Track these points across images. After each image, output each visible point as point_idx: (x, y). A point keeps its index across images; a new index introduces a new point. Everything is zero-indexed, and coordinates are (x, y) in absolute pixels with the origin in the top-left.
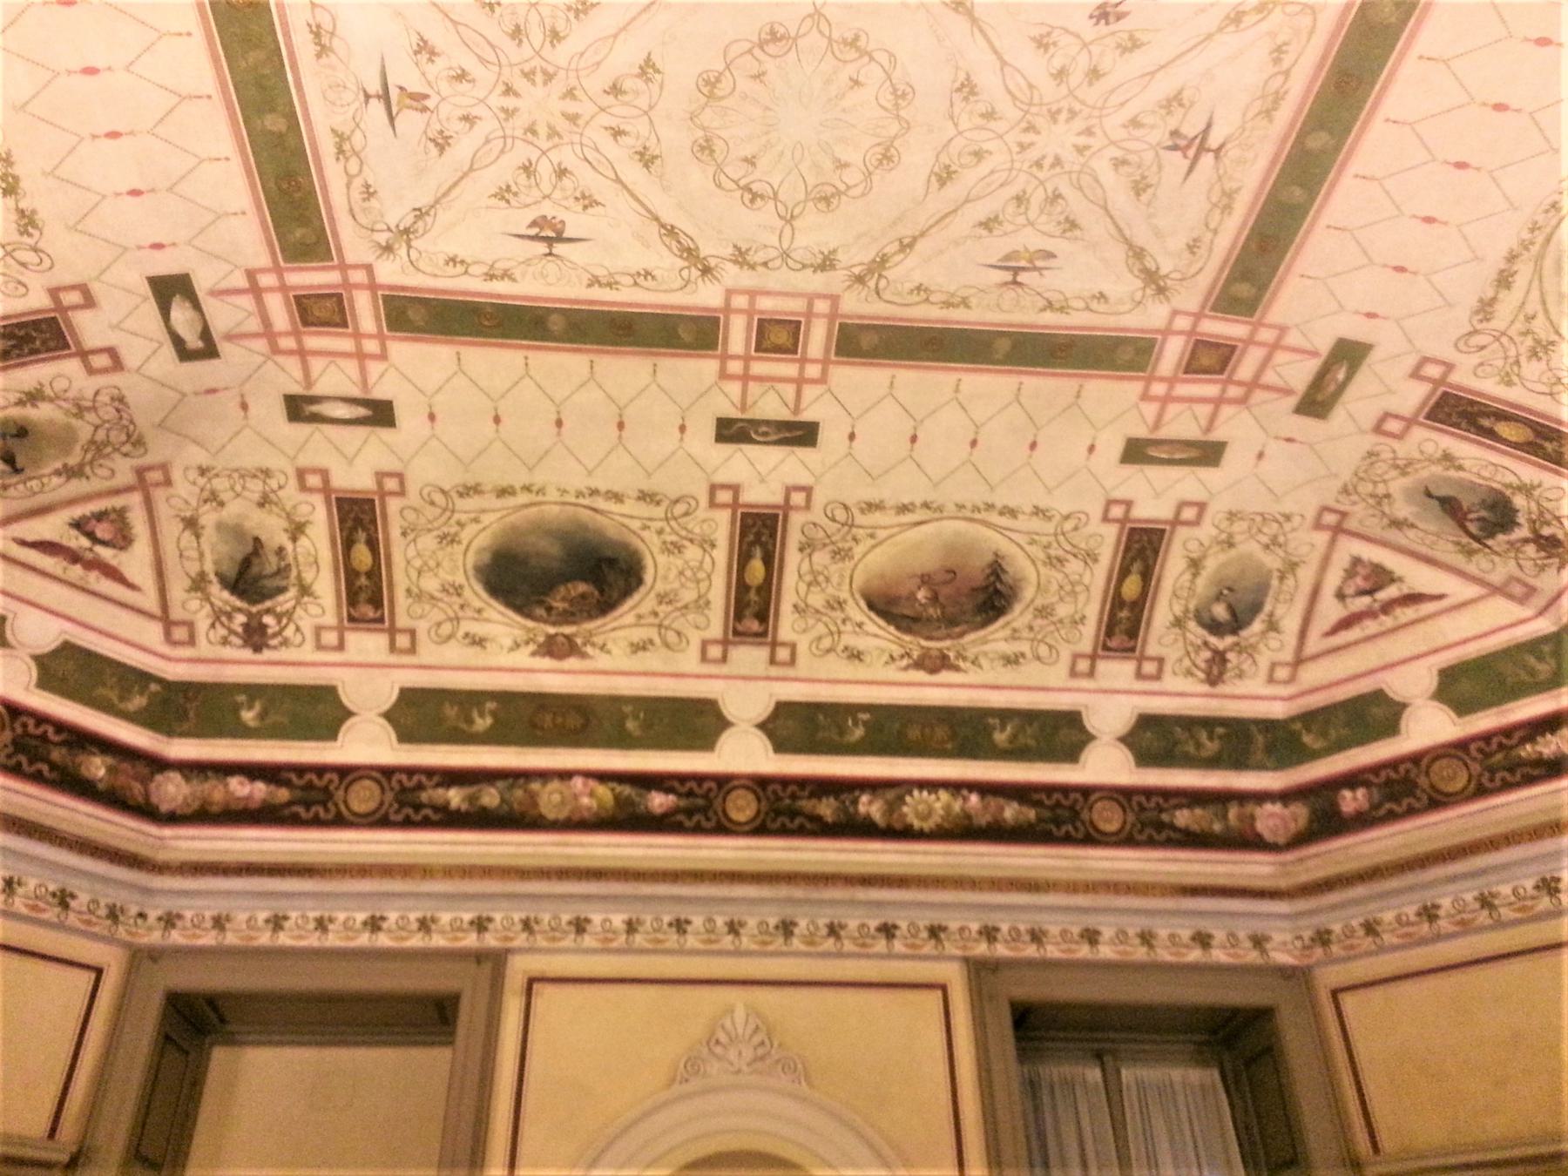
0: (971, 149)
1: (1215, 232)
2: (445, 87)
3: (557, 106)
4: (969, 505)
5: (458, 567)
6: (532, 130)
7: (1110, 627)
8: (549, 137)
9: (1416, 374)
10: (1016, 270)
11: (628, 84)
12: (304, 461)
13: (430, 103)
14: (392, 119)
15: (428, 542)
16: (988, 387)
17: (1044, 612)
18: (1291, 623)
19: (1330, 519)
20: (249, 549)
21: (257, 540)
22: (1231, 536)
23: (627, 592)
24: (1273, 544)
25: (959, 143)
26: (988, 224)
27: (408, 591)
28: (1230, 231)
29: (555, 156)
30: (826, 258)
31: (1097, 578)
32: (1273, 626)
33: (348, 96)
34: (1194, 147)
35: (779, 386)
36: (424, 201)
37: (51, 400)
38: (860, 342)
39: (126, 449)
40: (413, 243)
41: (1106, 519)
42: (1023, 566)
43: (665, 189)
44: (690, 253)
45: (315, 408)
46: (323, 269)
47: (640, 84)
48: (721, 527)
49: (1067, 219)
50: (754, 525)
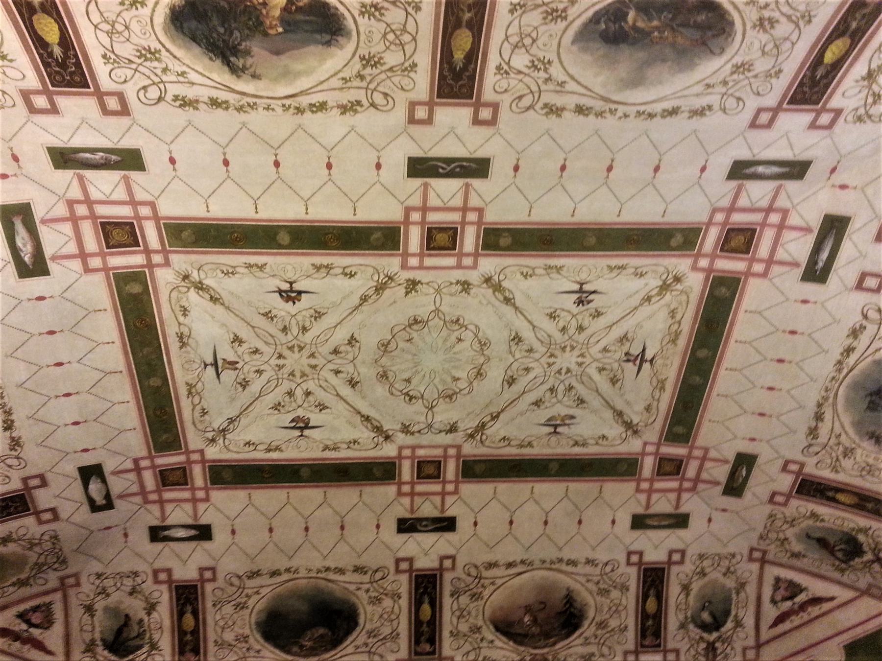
0: (523, 367)
1: (658, 400)
2: (247, 358)
3: (305, 361)
4: (548, 561)
5: (246, 623)
6: (292, 374)
7: (643, 632)
8: (301, 377)
9: (784, 469)
10: (556, 426)
11: (342, 349)
12: (158, 565)
13: (239, 366)
14: (218, 375)
15: (228, 609)
16: (549, 491)
17: (602, 625)
18: (749, 621)
19: (757, 555)
20: (122, 623)
21: (127, 616)
22: (703, 569)
23: (348, 632)
24: (727, 572)
25: (515, 366)
26: (537, 403)
27: (215, 641)
28: (666, 400)
29: (304, 386)
30: (452, 427)
31: (630, 600)
32: (738, 624)
33: (196, 366)
34: (640, 359)
35: (431, 497)
36: (233, 413)
37: (15, 541)
38: (476, 470)
39: (56, 566)
40: (227, 436)
41: (629, 563)
42: (586, 596)
43: (363, 398)
44: (378, 429)
45: (166, 533)
46: (176, 454)
47: (349, 348)
48: (403, 584)
49: (578, 398)
50: (422, 583)
